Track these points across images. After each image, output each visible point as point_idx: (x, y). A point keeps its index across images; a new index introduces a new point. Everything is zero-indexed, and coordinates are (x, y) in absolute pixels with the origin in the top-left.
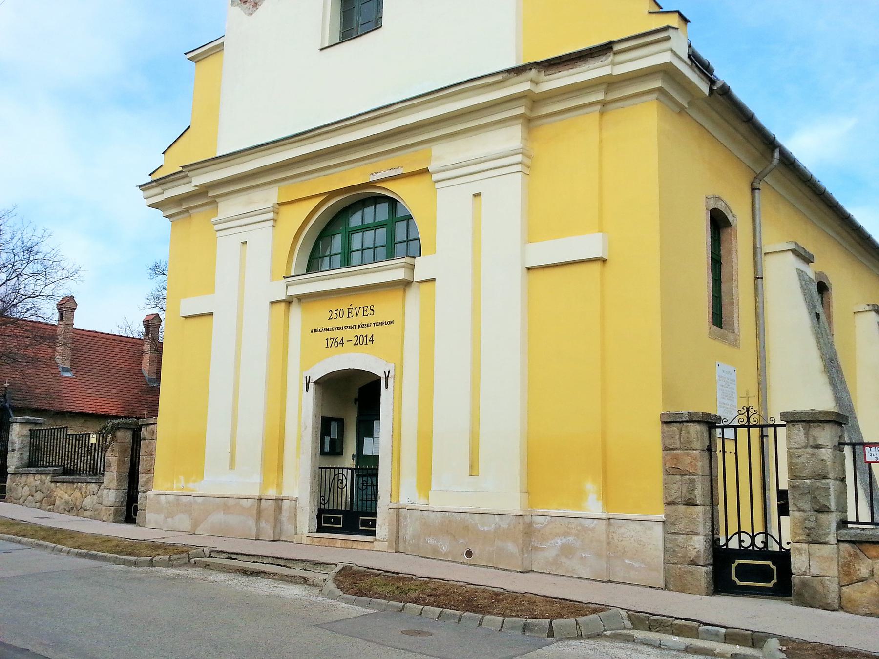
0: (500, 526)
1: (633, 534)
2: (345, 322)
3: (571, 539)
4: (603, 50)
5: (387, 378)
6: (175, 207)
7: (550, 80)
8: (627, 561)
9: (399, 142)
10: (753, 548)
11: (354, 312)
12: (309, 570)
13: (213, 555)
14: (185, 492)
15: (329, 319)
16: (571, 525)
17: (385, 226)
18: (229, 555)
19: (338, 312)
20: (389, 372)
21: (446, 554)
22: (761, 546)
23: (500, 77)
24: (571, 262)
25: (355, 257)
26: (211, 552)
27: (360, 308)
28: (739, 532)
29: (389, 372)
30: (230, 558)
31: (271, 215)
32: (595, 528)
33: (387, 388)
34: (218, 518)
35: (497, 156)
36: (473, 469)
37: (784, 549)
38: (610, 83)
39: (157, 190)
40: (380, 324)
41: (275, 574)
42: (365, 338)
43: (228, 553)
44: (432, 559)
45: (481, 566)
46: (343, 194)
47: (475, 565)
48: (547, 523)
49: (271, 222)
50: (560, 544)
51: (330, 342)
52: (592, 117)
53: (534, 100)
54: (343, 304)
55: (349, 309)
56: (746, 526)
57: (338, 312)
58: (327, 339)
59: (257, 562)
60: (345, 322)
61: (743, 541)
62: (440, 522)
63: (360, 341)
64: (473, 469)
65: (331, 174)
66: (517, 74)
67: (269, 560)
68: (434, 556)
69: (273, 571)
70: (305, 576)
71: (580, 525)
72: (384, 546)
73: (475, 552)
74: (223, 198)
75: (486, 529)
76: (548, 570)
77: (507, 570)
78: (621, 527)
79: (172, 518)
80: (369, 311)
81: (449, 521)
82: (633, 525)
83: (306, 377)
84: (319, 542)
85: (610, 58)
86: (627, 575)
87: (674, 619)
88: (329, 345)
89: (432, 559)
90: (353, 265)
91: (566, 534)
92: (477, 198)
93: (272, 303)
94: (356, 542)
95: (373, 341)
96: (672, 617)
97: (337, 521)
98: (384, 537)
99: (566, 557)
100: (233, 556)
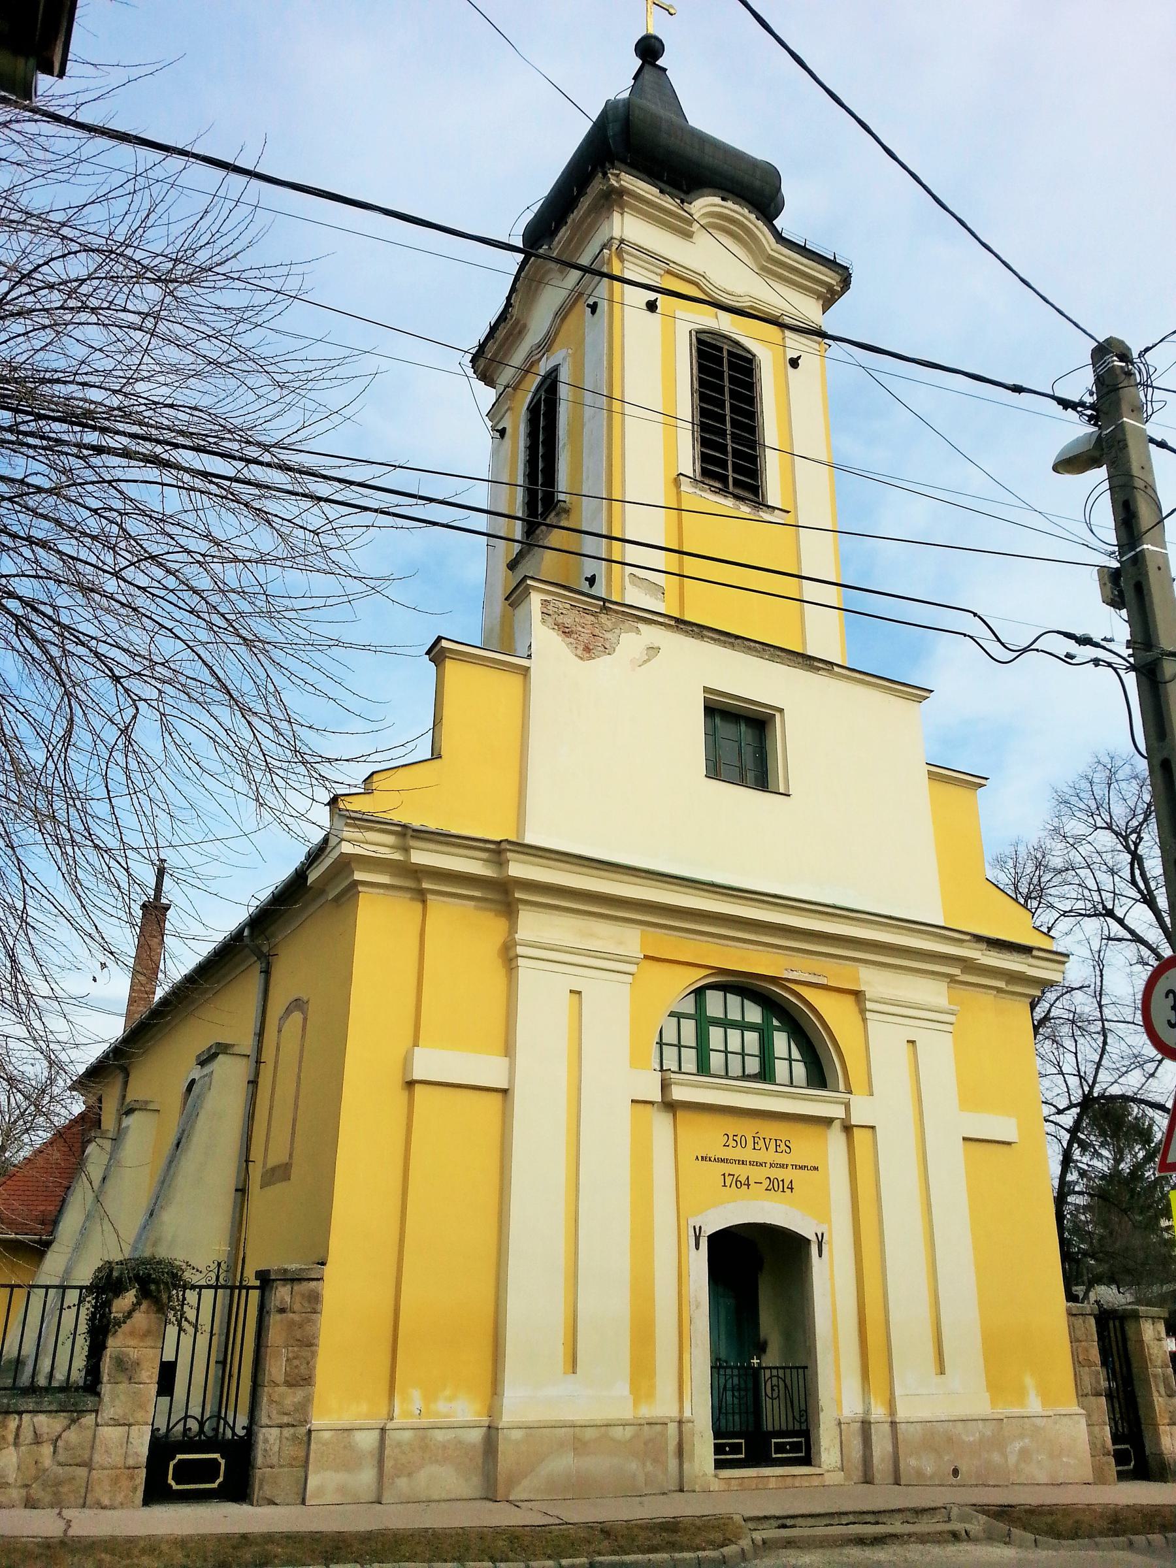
2: (748, 1154)
3: (1027, 1441)
6: (392, 875)
8: (1064, 1460)
11: (761, 1142)
18: (780, 1522)
20: (823, 1234)
21: (931, 1478)
22: (210, 1434)
23: (968, 938)
28: (186, 1417)
29: (823, 1234)
30: (784, 1526)
33: (820, 1256)
34: (563, 1464)
37: (237, 1436)
39: (390, 839)
40: (801, 1168)
41: (910, 1535)
42: (781, 1183)
43: (778, 1518)
51: (729, 1180)
52: (988, 998)
53: (967, 965)
54: (747, 1128)
56: (195, 1410)
58: (724, 1175)
59: (832, 1525)
60: (748, 1154)
61: (190, 1429)
63: (774, 1186)
67: (851, 1518)
72: (837, 1478)
73: (963, 1469)
74: (529, 908)
75: (972, 1439)
79: (410, 1475)
80: (783, 1147)
84: (740, 1485)
88: (728, 1184)
95: (792, 1189)
97: (780, 1448)
100: (789, 1522)
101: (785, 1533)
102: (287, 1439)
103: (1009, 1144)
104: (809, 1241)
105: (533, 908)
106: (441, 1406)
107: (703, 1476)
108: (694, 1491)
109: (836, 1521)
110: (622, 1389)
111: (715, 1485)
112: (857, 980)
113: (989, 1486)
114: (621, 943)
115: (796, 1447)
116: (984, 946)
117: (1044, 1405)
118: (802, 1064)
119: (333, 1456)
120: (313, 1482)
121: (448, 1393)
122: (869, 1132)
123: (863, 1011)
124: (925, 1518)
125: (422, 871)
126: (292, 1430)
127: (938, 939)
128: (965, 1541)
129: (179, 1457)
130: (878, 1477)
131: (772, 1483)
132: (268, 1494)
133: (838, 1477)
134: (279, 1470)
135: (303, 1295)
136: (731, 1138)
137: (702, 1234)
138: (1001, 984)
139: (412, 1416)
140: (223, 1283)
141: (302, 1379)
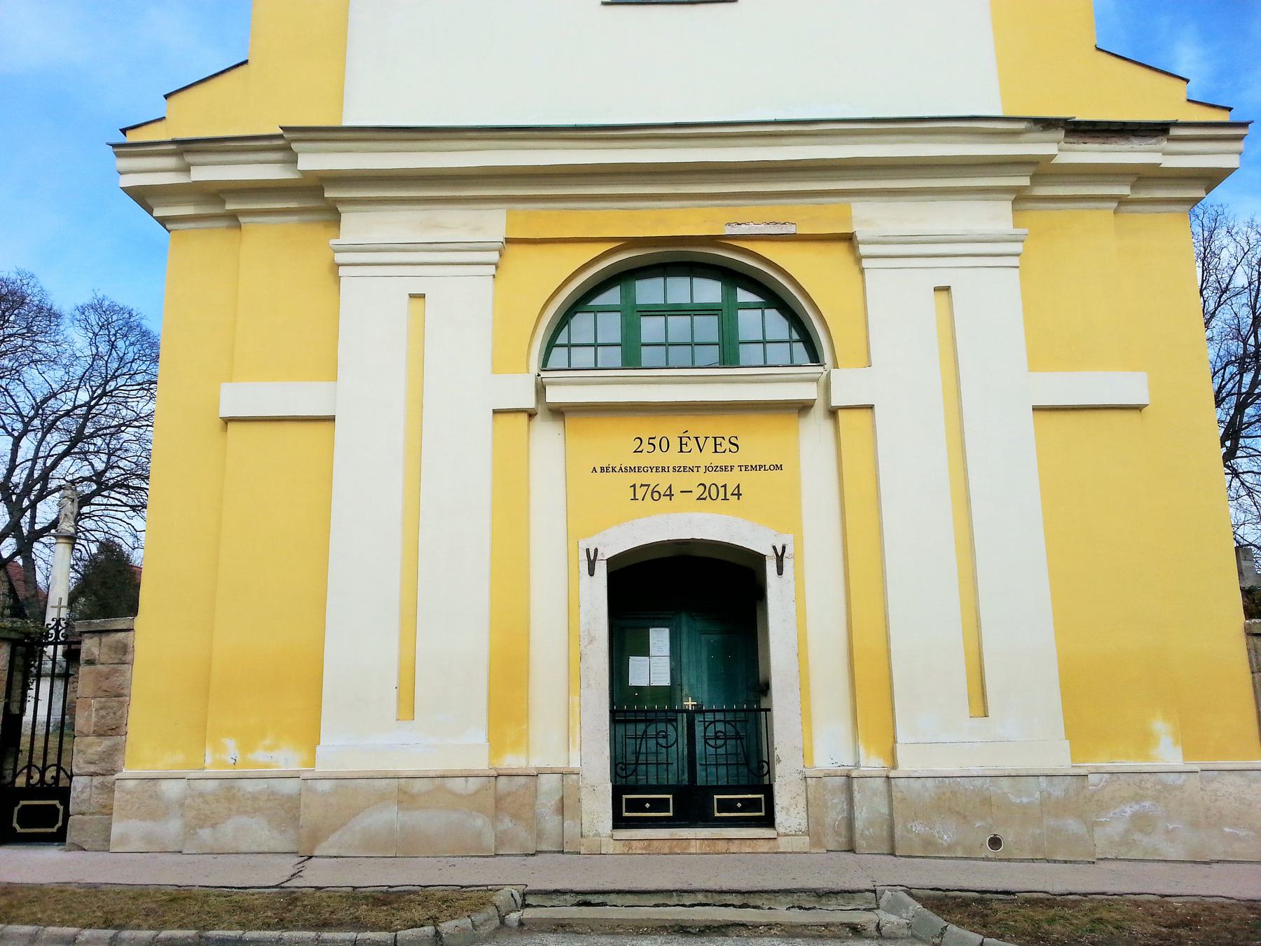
0: (1050, 795)
1: (1231, 789)
2: (673, 458)
3: (1147, 804)
4: (1155, 130)
5: (780, 560)
6: (196, 203)
7: (1071, 151)
8: (1227, 830)
9: (804, 183)
10: (42, 785)
11: (692, 444)
12: (809, 909)
13: (530, 900)
14: (251, 771)
15: (635, 452)
16: (1145, 783)
17: (716, 312)
18: (581, 898)
19: (656, 442)
20: (784, 548)
21: (950, 847)
23: (1021, 126)
24: (280, 418)
25: (749, 353)
26: (524, 895)
27: (706, 438)
29: (784, 548)
31: (494, 256)
32: (1183, 785)
33: (780, 571)
34: (386, 817)
35: (980, 238)
36: (981, 704)
37: (47, 784)
38: (1144, 176)
39: (171, 162)
41: (769, 926)
42: (722, 490)
43: (578, 893)
44: (923, 857)
45: (1022, 860)
46: (649, 247)
47: (1009, 860)
48: (1105, 784)
49: (492, 269)
50: (1130, 813)
51: (640, 492)
52: (1103, 216)
53: (1041, 169)
54: (671, 428)
55: (681, 438)
57: (656, 442)
58: (634, 486)
60: (673, 458)
62: (933, 795)
63: (707, 494)
64: (981, 704)
65: (636, 209)
66: (1043, 128)
67: (700, 898)
68: (930, 850)
69: (764, 920)
70: (856, 921)
71: (1161, 782)
72: (803, 843)
73: (1008, 837)
75: (1025, 800)
76: (1114, 854)
77: (1071, 862)
78: (1212, 781)
79: (214, 826)
80: (726, 445)
81: (952, 792)
82: (1230, 778)
83: (588, 551)
85: (1165, 145)
86: (1230, 849)
87: (314, 889)
88: (639, 495)
89: (923, 857)
90: (643, 365)
91: (1138, 798)
92: (419, 302)
93: (495, 412)
94: (737, 842)
95: (739, 495)
96: (459, 886)
98: (794, 827)
99: (1141, 831)
101: (587, 912)
102: (96, 787)
103: (1138, 408)
104: (761, 559)
105: (373, 207)
106: (260, 756)
107: (595, 835)
108: (579, 853)
109: (675, 900)
110: (478, 736)
111: (609, 847)
112: (848, 219)
113: (1055, 861)
114: (478, 229)
115: (751, 805)
116: (1061, 134)
117: (1186, 756)
118: (801, 344)
119: (137, 805)
120: (117, 829)
121: (267, 742)
122: (861, 417)
123: (858, 259)
124: (833, 903)
125: (222, 191)
126: (100, 779)
127: (970, 138)
128: (872, 938)
129: (22, 803)
130: (861, 843)
131: (694, 847)
132: (76, 840)
133: (803, 843)
134: (90, 817)
135: (110, 648)
136: (645, 441)
137: (599, 557)
138: (1125, 191)
139: (227, 766)
140: (62, 639)
141: (113, 729)
